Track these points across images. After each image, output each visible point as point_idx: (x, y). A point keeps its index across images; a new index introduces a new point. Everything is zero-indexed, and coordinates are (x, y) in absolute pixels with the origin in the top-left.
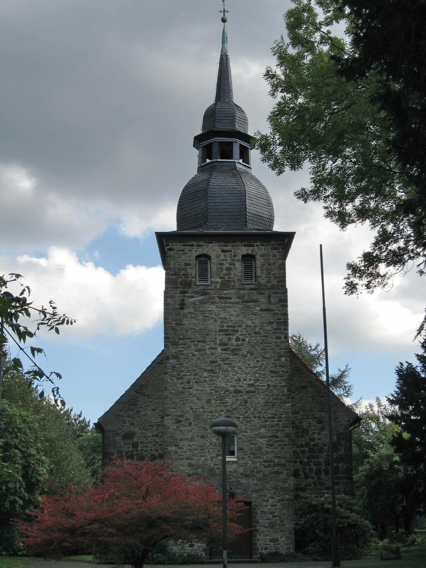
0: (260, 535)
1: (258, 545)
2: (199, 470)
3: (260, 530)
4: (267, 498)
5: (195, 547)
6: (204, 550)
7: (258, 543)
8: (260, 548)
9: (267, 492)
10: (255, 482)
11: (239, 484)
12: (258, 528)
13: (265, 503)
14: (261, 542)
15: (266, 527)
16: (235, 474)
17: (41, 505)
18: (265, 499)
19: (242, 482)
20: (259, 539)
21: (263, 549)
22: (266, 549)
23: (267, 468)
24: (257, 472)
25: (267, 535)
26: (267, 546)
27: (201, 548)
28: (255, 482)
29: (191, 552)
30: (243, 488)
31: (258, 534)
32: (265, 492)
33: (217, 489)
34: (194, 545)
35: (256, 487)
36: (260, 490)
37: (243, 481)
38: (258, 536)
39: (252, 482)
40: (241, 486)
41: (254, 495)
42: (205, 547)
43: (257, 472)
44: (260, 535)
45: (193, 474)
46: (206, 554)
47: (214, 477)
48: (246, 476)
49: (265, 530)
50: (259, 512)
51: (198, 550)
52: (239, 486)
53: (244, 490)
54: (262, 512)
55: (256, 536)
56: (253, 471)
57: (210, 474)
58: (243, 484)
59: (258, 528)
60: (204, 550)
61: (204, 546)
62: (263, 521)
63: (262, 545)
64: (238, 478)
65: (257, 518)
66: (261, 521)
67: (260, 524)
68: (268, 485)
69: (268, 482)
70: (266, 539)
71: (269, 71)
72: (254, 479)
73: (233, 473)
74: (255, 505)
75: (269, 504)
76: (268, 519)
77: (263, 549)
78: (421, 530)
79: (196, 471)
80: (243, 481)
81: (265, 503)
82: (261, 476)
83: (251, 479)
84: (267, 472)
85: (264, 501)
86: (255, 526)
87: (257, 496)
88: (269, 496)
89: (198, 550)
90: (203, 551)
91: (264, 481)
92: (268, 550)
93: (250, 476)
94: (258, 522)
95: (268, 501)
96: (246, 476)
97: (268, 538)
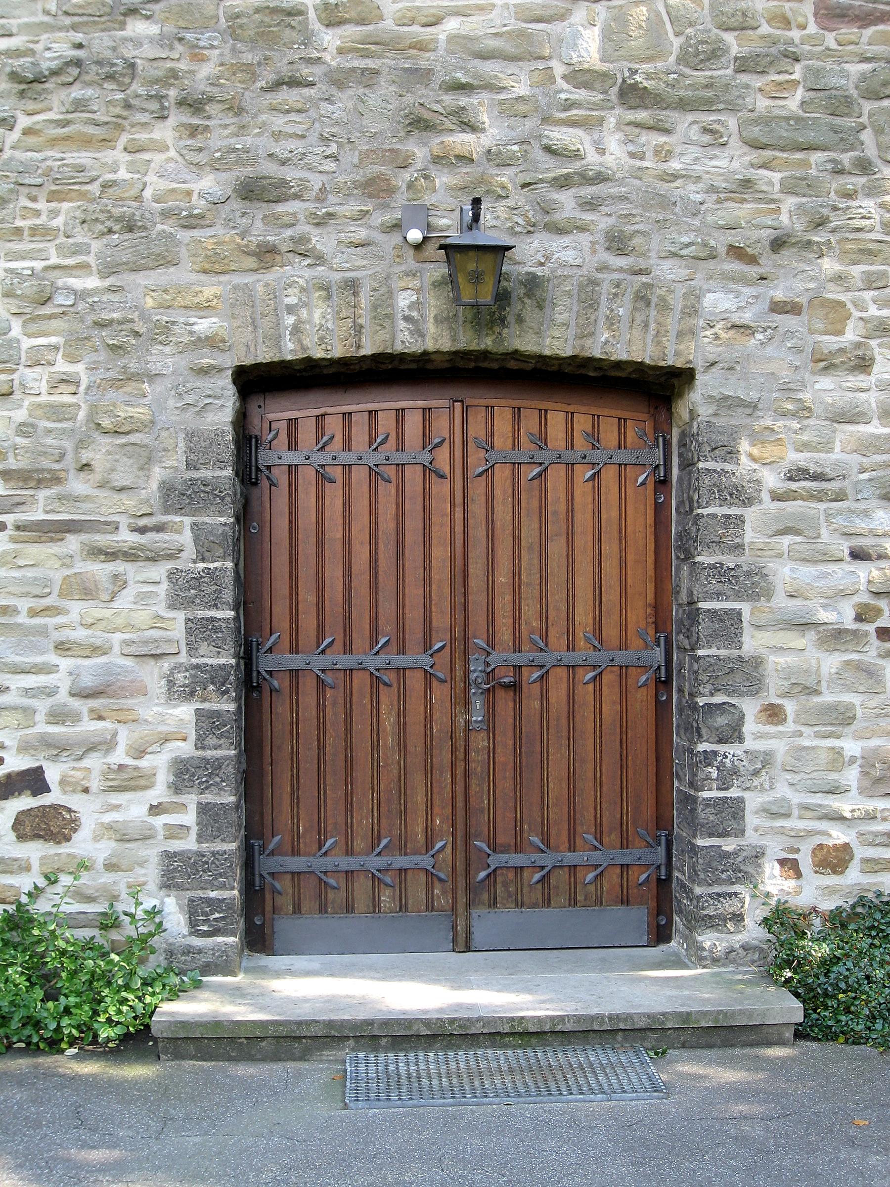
0: (774, 714)
1: (752, 820)
2: (138, 27)
3: (775, 661)
4: (851, 335)
5: (84, 844)
6: (178, 872)
7: (753, 801)
8: (775, 848)
9: (857, 270)
10: (734, 161)
11: (563, 183)
12: (752, 642)
13: (825, 383)
14: (782, 790)
15: (836, 637)
16: (520, 84)
17: (838, 953)
18: (830, 342)
19: (592, 157)
20: (767, 759)
21: (806, 862)
22: (834, 860)
23: (849, 31)
24: (744, 65)
25: (842, 718)
26: (838, 835)
27: (152, 853)
28: (734, 161)
29: (35, 893)
30: (602, 222)
31: (750, 707)
32: (829, 265)
33: (321, 222)
34: (73, 824)
35: (742, 211)
36: (778, 244)
37: (609, 148)
38: (750, 727)
39: (701, 160)
40: (590, 205)
41: (718, 301)
42: (189, 844)
43: (744, 65)
44: (774, 714)
45: (73, 67)
46: (195, 912)
47: (290, 96)
48: (631, 94)
49: (831, 662)
50: (771, 480)
51: (110, 867)
52: (566, 202)
53: (618, 243)
54: (797, 474)
55: (734, 734)
56: (716, 53)
57: (250, 72)
58: (601, 178)
59: (752, 642)
60: (178, 872)
61: (176, 832)
62: (807, 572)
63: (795, 823)
64: (546, 120)
65: (750, 536)
66: (784, 573)
67: (780, 601)
68: (868, 204)
69: (864, 166)
70: (838, 760)
71: (512, 228)
72: (715, 138)
73: (490, 68)
74: (726, 403)
75: (872, 400)
76: (858, 555)
77: (806, 862)
78: (213, 894)
79: (100, 42)
80: (609, 148)
81: (826, 389)
82: (793, 103)
83: (686, 124)
84: (856, 69)
85: (826, 363)
86: (729, 626)
87: (747, 317)
88: (873, 311)
89: (110, 867)
90: (168, 883)
91: (816, 157)
92: (854, 876)
93: (683, 105)
94: (752, 584)
95: (864, 365)
96: (631, 94)
97: (851, 747)
